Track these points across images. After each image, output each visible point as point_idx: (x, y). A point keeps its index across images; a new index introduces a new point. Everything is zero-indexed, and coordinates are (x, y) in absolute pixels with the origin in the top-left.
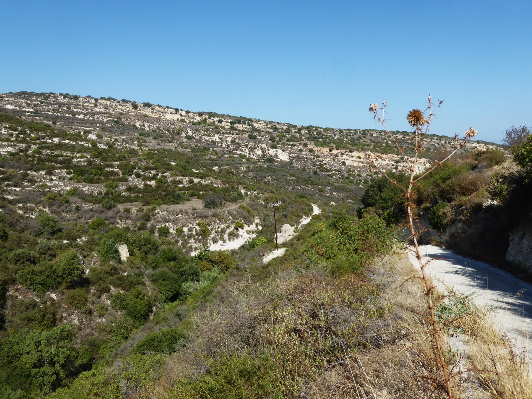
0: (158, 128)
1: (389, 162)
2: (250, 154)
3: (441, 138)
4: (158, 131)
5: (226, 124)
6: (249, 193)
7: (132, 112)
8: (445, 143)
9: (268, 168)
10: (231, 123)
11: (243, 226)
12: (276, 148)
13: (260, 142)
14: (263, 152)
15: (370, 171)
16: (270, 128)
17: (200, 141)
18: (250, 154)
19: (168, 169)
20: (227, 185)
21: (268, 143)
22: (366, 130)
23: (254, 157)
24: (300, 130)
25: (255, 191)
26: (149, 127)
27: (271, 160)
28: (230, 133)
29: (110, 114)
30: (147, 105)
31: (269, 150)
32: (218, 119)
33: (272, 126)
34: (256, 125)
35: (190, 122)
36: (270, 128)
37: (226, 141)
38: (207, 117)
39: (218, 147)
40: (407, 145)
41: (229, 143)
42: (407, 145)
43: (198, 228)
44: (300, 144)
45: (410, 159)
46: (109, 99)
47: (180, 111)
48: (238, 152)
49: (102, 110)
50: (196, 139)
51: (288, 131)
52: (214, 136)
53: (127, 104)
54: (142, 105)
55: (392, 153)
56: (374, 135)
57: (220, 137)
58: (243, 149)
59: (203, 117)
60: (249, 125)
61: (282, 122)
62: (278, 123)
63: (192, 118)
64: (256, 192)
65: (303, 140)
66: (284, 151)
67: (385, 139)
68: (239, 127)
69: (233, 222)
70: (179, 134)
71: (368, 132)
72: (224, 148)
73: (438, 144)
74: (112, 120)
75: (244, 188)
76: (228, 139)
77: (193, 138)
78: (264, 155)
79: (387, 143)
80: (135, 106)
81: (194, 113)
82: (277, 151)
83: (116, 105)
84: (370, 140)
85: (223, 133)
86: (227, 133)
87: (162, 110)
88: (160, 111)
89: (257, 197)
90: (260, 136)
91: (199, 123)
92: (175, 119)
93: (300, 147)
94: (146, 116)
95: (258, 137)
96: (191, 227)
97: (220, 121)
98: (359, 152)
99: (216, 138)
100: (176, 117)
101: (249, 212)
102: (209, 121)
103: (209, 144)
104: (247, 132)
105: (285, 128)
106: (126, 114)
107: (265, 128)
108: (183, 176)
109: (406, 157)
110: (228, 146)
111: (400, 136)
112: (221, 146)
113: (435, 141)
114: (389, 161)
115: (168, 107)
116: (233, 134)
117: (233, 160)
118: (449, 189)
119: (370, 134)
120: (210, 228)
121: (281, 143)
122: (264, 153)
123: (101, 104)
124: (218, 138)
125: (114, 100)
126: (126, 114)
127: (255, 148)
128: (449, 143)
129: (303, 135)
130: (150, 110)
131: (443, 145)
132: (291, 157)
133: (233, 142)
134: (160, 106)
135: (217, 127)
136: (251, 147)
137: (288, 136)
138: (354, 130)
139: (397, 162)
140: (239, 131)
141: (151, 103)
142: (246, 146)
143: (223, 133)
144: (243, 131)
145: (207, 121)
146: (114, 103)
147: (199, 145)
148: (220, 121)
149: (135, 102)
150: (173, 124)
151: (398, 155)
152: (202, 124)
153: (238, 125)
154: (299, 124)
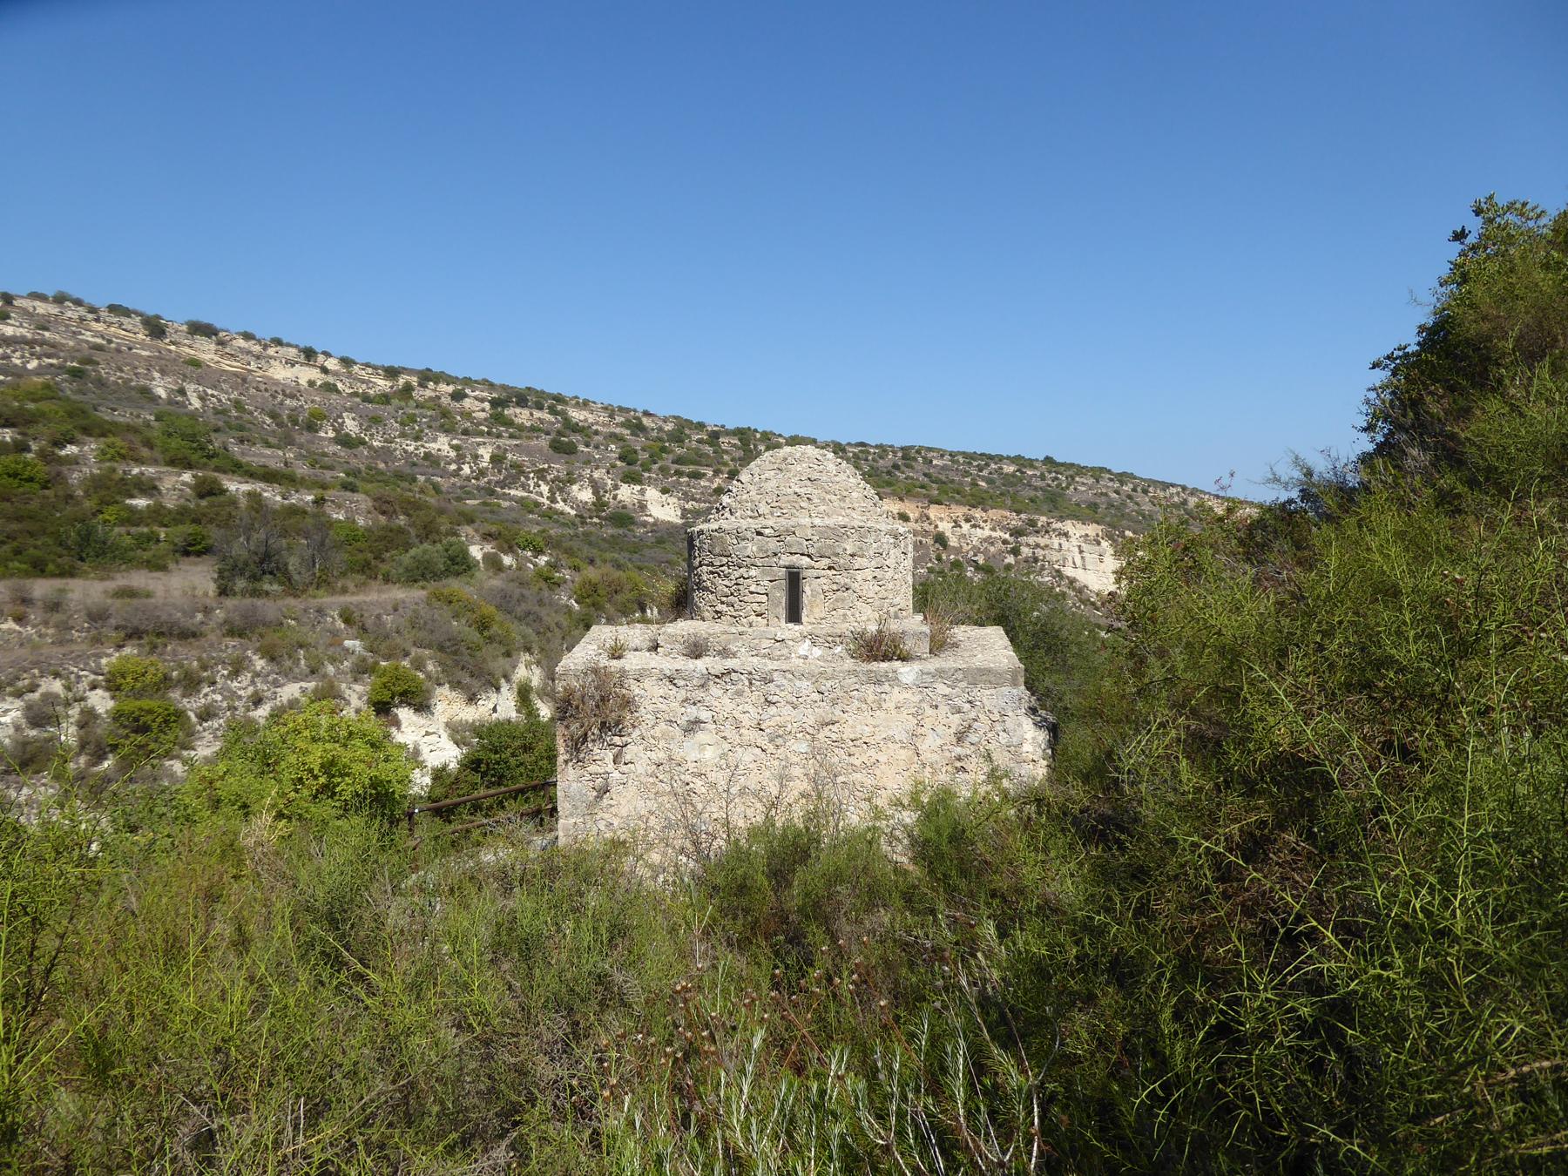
0: (238, 405)
1: (994, 534)
2: (553, 500)
3: (1123, 477)
4: (234, 413)
5: (476, 406)
6: (507, 560)
7: (143, 346)
8: (1134, 490)
9: (614, 542)
10: (495, 403)
11: (428, 694)
12: (640, 482)
13: (587, 462)
14: (596, 493)
15: (939, 559)
16: (622, 425)
17: (385, 453)
18: (553, 500)
19: (86, 431)
20: (402, 520)
21: (613, 466)
22: (912, 447)
23: (568, 509)
24: (715, 436)
25: (538, 552)
26: (202, 398)
27: (623, 518)
28: (489, 433)
29: (53, 346)
30: (200, 329)
31: (616, 487)
32: (450, 389)
33: (628, 420)
34: (576, 415)
35: (356, 394)
36: (622, 425)
37: (476, 457)
38: (414, 380)
39: (445, 474)
40: (1032, 493)
41: (485, 462)
42: (1032, 493)
43: (101, 702)
44: (717, 473)
45: (1054, 526)
46: (60, 299)
47: (321, 358)
48: (513, 492)
49: (25, 332)
50: (371, 448)
51: (678, 437)
52: (435, 440)
53: (125, 320)
54: (185, 328)
55: (1000, 507)
57: (455, 442)
58: (531, 483)
59: (401, 381)
60: (553, 411)
61: (661, 414)
62: (646, 414)
63: (363, 382)
64: (543, 560)
65: (725, 464)
66: (664, 491)
67: (967, 474)
68: (522, 416)
69: (362, 670)
70: (311, 427)
71: (918, 452)
72: (468, 479)
73: (1117, 492)
74: (60, 367)
75: (487, 537)
76: (481, 451)
77: (363, 443)
78: (600, 505)
79: (974, 484)
80: (156, 328)
81: (368, 365)
82: (642, 492)
83: (82, 319)
85: (466, 432)
86: (481, 434)
87: (257, 349)
88: (249, 352)
89: (553, 584)
90: (587, 446)
91: (385, 399)
92: (303, 382)
93: (717, 482)
94: (195, 363)
95: (582, 448)
96: (50, 698)
97: (458, 396)
98: (901, 499)
99: (442, 445)
100: (311, 374)
101: (483, 625)
102: (421, 394)
103: (414, 464)
104: (548, 433)
105: (669, 427)
106: (118, 351)
107: (604, 425)
108: (172, 462)
109: (1044, 519)
110: (482, 473)
111: (1009, 469)
112: (456, 473)
113: (1106, 484)
114: (993, 529)
115: (278, 342)
116: (499, 436)
117: (492, 512)
118: (211, 995)
120: (191, 706)
121: (655, 467)
122: (599, 498)
123: (25, 312)
124: (446, 447)
125: (78, 303)
126: (118, 351)
127: (572, 482)
128: (1145, 492)
129: (726, 452)
130: (213, 347)
131: (1129, 497)
132: (690, 511)
133: (497, 460)
134: (248, 336)
135: (445, 414)
136: (557, 479)
137: (678, 451)
138: (876, 447)
139: (1017, 533)
140: (521, 428)
141: (218, 325)
142: (541, 475)
143: (466, 432)
144: (533, 429)
145: (409, 398)
146: (73, 313)
147: (382, 466)
148: (458, 396)
149: (159, 317)
150: (292, 396)
151: (1018, 512)
152: (395, 402)
153: (518, 410)
154: (712, 420)
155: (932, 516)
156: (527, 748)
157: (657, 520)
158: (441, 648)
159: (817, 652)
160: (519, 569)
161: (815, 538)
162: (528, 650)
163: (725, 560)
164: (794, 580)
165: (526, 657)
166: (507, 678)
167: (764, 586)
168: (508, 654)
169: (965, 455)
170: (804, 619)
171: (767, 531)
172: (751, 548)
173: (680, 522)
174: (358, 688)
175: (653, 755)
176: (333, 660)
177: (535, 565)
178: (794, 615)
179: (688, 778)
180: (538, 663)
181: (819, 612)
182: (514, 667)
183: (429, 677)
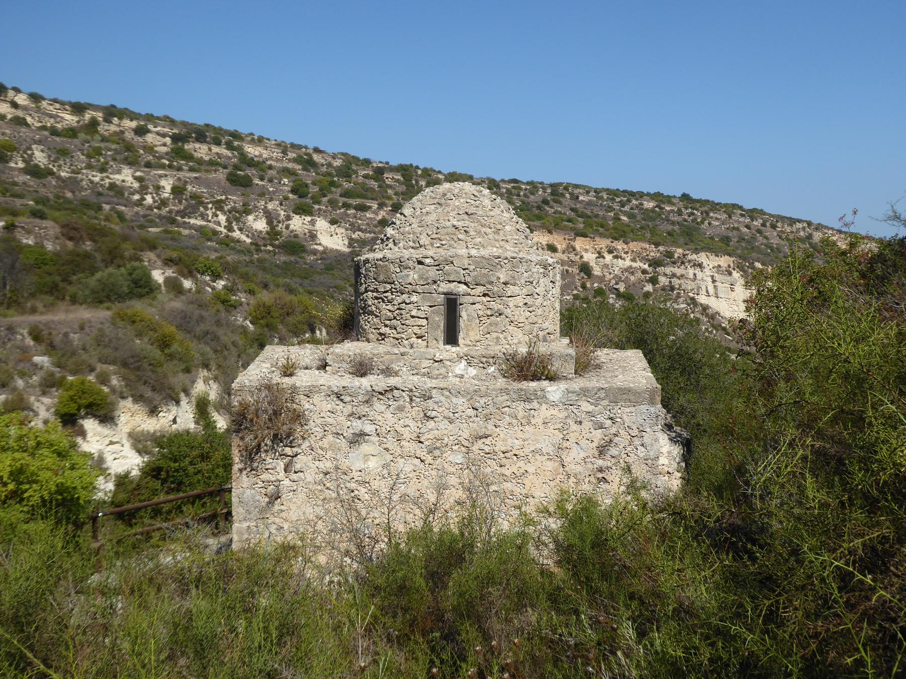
6: (187, 284)
20: (88, 246)
25: (216, 276)
56: (581, 198)
58: (210, 213)
60: (229, 146)
64: (220, 284)
67: (610, 209)
69: (49, 384)
75: (168, 262)
79: (617, 219)
84: (572, 209)
98: (550, 232)
101: (164, 343)
119: (571, 194)
127: (248, 212)
138: (528, 183)
144: (211, 163)
155: (578, 248)
156: (204, 457)
157: (326, 248)
158: (125, 364)
159: (472, 371)
160: (198, 292)
161: (472, 267)
162: (206, 366)
163: (388, 287)
164: (452, 305)
165: (204, 373)
166: (187, 392)
167: (424, 310)
168: (187, 370)
169: (608, 191)
170: (461, 341)
171: (427, 261)
172: (413, 276)
173: (347, 250)
174: (47, 400)
175: (321, 465)
176: (22, 375)
177: (213, 288)
178: (451, 338)
179: (353, 485)
180: (216, 379)
181: (474, 335)
182: (193, 382)
183: (113, 391)
